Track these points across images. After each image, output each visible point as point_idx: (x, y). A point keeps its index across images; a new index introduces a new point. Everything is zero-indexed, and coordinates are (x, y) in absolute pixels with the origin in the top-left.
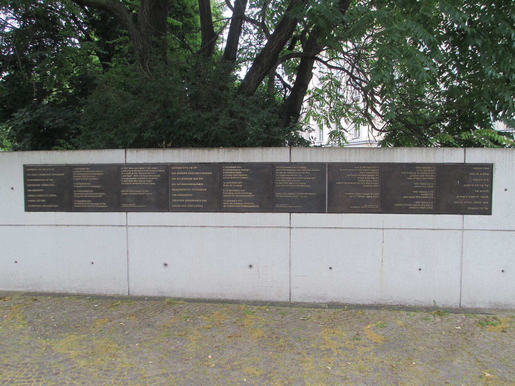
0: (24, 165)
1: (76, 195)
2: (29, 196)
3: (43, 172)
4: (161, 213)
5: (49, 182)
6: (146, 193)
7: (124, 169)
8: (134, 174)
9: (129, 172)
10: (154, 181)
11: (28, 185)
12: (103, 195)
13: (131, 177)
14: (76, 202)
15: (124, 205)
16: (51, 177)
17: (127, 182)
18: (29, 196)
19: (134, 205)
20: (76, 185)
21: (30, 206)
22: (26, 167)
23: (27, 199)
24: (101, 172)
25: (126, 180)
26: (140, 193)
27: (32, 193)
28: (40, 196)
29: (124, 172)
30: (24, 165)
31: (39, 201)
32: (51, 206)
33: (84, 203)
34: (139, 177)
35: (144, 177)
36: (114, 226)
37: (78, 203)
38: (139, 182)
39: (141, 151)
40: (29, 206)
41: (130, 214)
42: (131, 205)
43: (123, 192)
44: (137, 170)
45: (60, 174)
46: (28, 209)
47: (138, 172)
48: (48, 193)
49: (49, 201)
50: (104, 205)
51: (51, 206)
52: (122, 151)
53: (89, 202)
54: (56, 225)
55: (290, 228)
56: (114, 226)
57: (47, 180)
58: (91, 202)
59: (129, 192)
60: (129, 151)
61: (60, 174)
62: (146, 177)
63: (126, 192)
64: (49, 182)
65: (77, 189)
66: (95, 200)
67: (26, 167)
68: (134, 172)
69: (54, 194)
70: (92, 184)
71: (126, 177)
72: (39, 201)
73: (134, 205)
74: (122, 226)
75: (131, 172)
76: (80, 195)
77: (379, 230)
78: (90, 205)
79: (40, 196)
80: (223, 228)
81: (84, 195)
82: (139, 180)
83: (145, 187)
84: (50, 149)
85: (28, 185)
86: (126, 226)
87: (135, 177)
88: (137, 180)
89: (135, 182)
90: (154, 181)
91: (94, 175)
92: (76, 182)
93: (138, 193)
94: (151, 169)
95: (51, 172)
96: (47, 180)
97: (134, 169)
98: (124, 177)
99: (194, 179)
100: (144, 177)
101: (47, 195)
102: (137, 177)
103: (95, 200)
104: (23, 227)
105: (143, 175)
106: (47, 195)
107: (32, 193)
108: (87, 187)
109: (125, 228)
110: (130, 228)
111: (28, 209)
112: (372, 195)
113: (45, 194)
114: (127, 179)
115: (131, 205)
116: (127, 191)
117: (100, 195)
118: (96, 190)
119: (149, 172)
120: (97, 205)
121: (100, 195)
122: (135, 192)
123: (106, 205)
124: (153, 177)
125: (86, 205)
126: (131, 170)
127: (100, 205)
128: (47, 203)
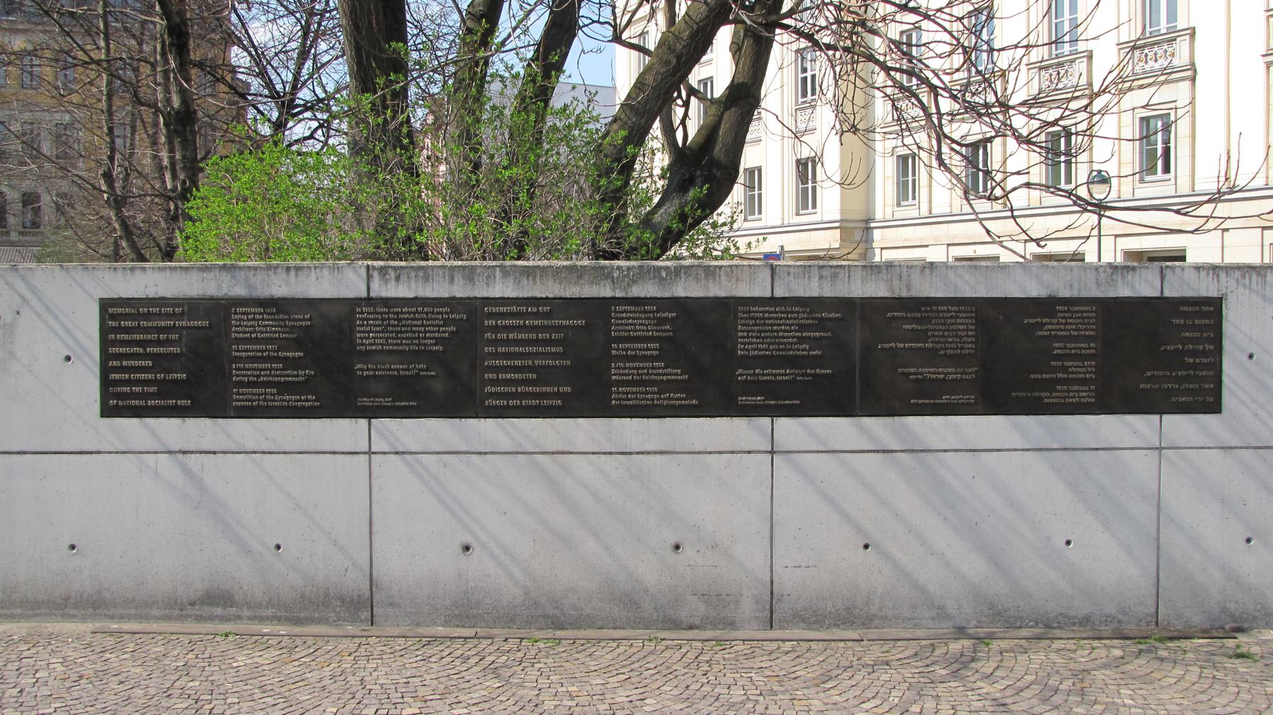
5: (168, 342)
10: (438, 341)
11: (112, 350)
19: (387, 401)
28: (143, 376)
29: (363, 319)
32: (172, 402)
33: (259, 395)
36: (334, 453)
37: (239, 398)
43: (362, 370)
46: (108, 411)
51: (172, 402)
55: (370, 453)
59: (377, 369)
63: (368, 370)
65: (238, 359)
66: (284, 388)
67: (105, 305)
75: (383, 320)
79: (143, 376)
81: (258, 376)
85: (112, 350)
93: (398, 370)
101: (160, 376)
102: (397, 332)
103: (284, 388)
108: (268, 357)
111: (108, 411)
114: (368, 336)
115: (380, 400)
120: (290, 399)
125: (265, 400)
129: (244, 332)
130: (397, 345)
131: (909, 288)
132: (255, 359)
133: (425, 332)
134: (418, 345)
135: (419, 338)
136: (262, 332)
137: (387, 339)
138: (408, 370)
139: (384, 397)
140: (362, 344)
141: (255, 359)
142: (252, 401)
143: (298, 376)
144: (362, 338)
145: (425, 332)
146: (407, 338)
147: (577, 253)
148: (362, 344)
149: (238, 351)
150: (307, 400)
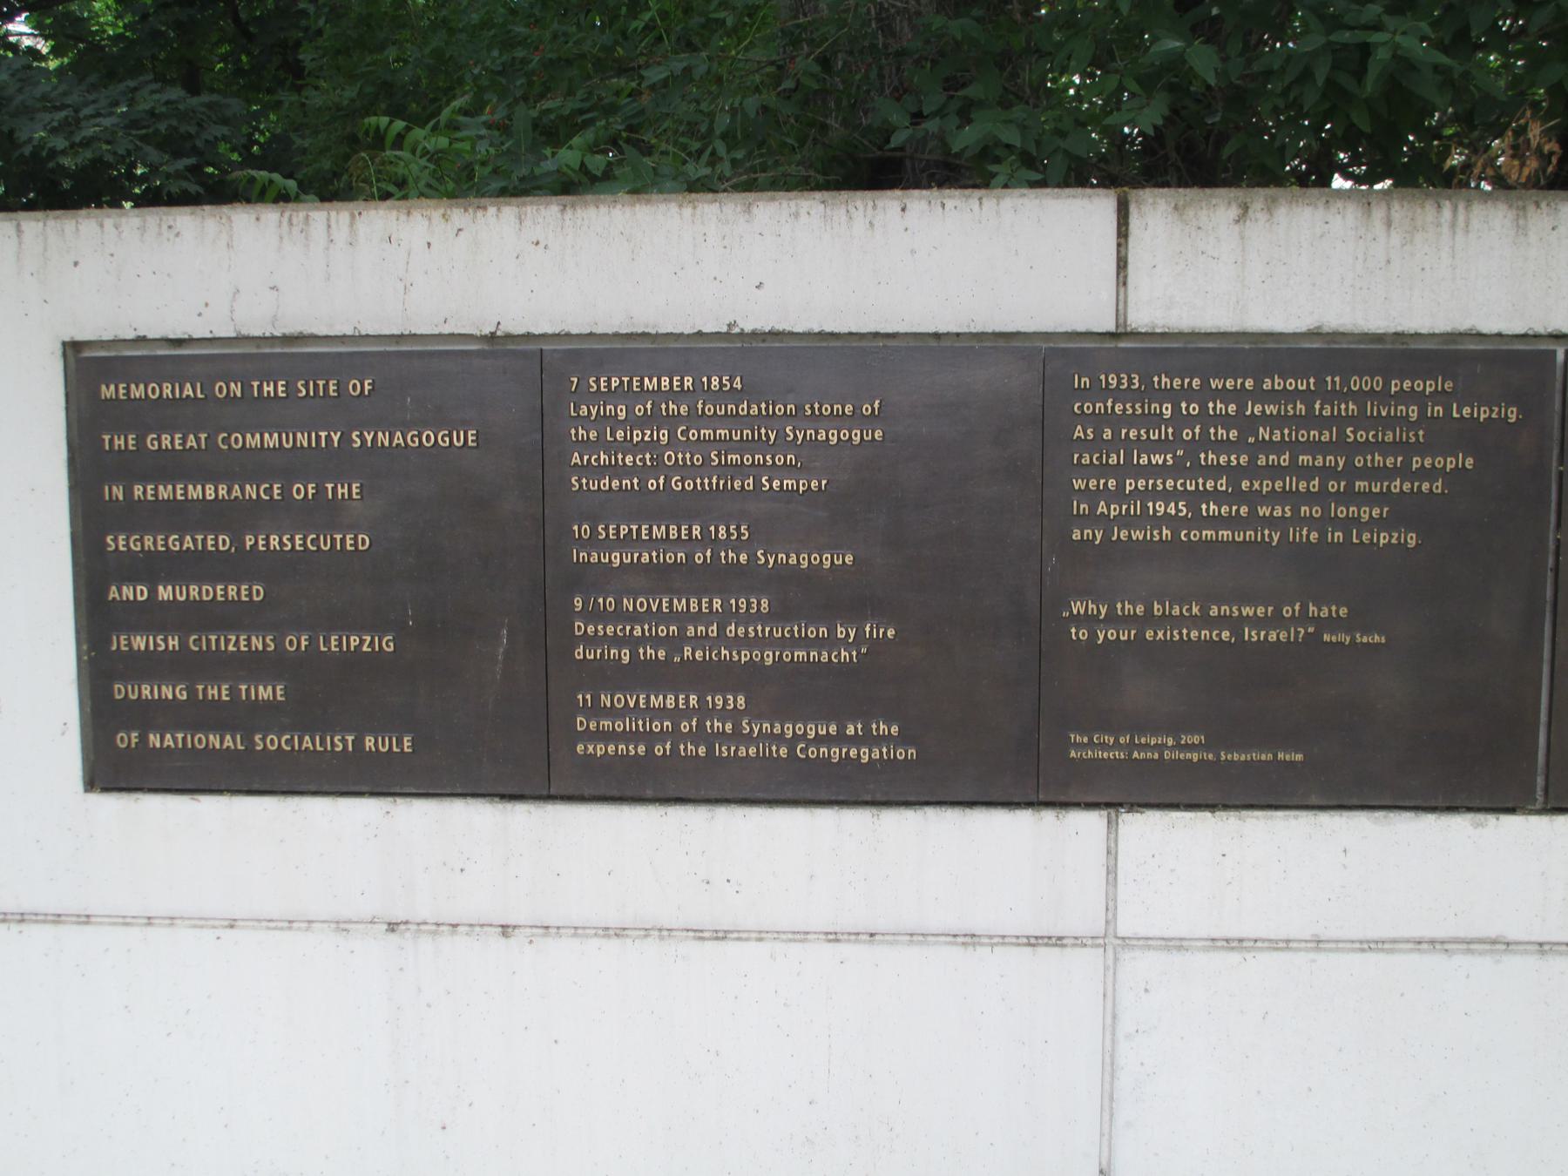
0: (73, 349)
1: (593, 638)
2: (120, 642)
3: (258, 413)
4: (1459, 824)
5: (324, 514)
6: (1322, 624)
7: (1098, 392)
8: (1205, 443)
9: (1156, 420)
10: (1403, 512)
11: (117, 542)
12: (877, 645)
13: (1177, 470)
14: (596, 711)
15: (1087, 747)
16: (337, 463)
17: (1126, 521)
18: (120, 642)
19: (1190, 747)
20: (593, 543)
21: (126, 750)
22: (87, 366)
23: (100, 670)
24: (857, 419)
25: (1119, 495)
26: (1260, 624)
27: (151, 616)
28: (235, 643)
29: (1099, 421)
30: (73, 349)
31: (218, 692)
32: (341, 742)
33: (676, 715)
34: (1252, 471)
35: (1307, 473)
36: (971, 939)
37: (612, 724)
38: (1253, 521)
39: (1282, 212)
40: (127, 739)
41: (1146, 831)
42: (1159, 746)
43: (1089, 620)
44: (1239, 396)
45: (429, 437)
46: (114, 766)
47: (1248, 424)
48: (329, 621)
49: (323, 694)
50: (881, 742)
51: (341, 742)
52: (1091, 211)
53: (735, 715)
54: (392, 927)
55: (1111, 941)
56: (971, 939)
57: (302, 491)
58: (753, 712)
59: (1148, 619)
60: (1156, 213)
61: (429, 437)
62: (1327, 473)
63: (1112, 619)
64: (324, 514)
65: (602, 578)
66: (788, 691)
67: (87, 366)
68: (1205, 418)
69: (378, 628)
70: (764, 533)
71: (1121, 472)
72: (218, 692)
73: (1190, 747)
74: (1058, 942)
75: (1179, 420)
76: (633, 643)
77: (1073, 955)
78: (737, 736)
79: (235, 643)
80: (730, 947)
81: (674, 644)
82: (1253, 498)
83: (1316, 569)
84: (331, 187)
85: (117, 542)
86: (1111, 941)
87: (1215, 471)
88: (1237, 496)
89: (1216, 522)
90: (1403, 512)
91: (782, 444)
92: (599, 509)
93: (1236, 624)
94: (1384, 397)
95: (342, 411)
96: (302, 491)
97: (1205, 394)
98: (1104, 470)
99: (165, 593)
100: (1307, 473)
101: (298, 642)
102: (1235, 473)
103: (788, 691)
104: (71, 934)
105: (1295, 447)
106: (298, 642)
107: (151, 616)
108: (713, 568)
109: (1086, 963)
110: (1138, 966)
111: (114, 766)
112: (855, 741)
113: (279, 629)
114: (1137, 494)
115: (1159, 746)
116: (1124, 608)
117: (844, 643)
118: (799, 596)
119: (1359, 421)
120: (810, 735)
121: (844, 643)
122: (1205, 621)
123: (904, 740)
124: (1404, 472)
125: (699, 736)
126: (1173, 396)
127: (841, 739)
128: (303, 712)
129: (616, 471)
130: (1232, 522)
131: (1128, 1037)
132: (662, 578)
133: (1351, 473)
134: (1321, 524)
135: (1322, 497)
136: (685, 470)
137: (1195, 499)
138: (1277, 621)
139: (1175, 729)
140: (1092, 519)
141: (662, 578)
142: (650, 738)
143: (831, 643)
144: (1092, 497)
145: (1351, 473)
146: (1273, 498)
147: (525, 98)
148: (1092, 519)
149: (608, 547)
150: (867, 739)
